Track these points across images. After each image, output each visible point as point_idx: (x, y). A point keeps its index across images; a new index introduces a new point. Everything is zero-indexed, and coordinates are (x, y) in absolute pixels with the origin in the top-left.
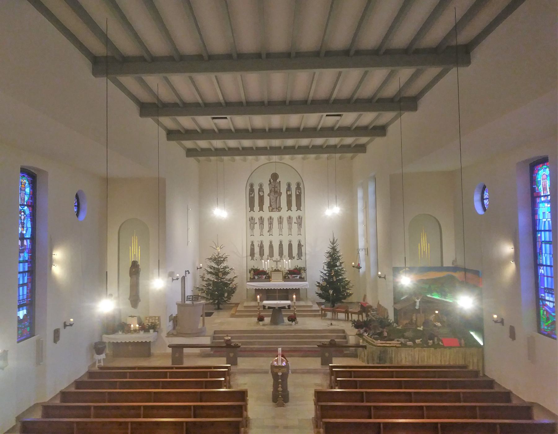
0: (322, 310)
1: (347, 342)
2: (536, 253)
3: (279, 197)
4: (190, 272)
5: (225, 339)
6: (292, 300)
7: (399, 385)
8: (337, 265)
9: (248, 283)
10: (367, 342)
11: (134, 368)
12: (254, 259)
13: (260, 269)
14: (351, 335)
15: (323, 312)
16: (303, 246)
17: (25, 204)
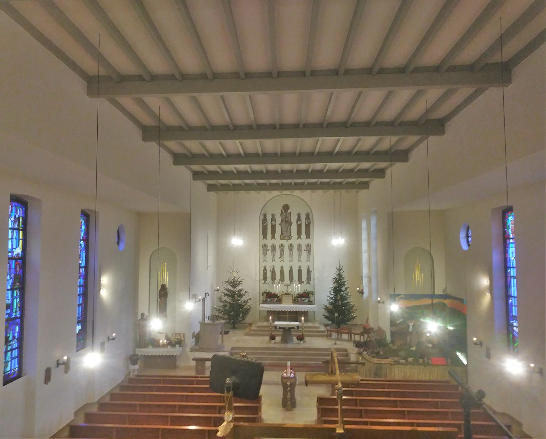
0: (328, 330)
1: (349, 359)
2: (507, 286)
3: (289, 226)
4: (210, 294)
5: (241, 355)
6: (300, 321)
7: (388, 394)
8: (343, 289)
9: (261, 305)
10: (366, 359)
11: (166, 376)
12: (267, 283)
13: (272, 293)
14: (352, 354)
15: (329, 333)
16: (311, 271)
17: (82, 239)
